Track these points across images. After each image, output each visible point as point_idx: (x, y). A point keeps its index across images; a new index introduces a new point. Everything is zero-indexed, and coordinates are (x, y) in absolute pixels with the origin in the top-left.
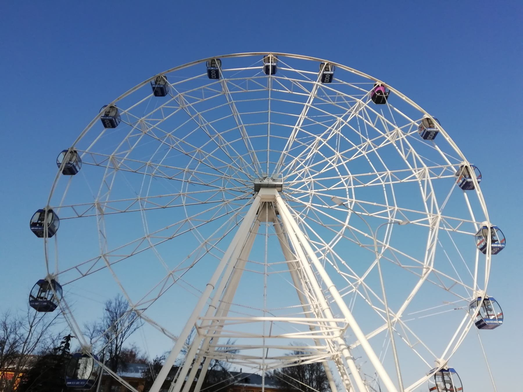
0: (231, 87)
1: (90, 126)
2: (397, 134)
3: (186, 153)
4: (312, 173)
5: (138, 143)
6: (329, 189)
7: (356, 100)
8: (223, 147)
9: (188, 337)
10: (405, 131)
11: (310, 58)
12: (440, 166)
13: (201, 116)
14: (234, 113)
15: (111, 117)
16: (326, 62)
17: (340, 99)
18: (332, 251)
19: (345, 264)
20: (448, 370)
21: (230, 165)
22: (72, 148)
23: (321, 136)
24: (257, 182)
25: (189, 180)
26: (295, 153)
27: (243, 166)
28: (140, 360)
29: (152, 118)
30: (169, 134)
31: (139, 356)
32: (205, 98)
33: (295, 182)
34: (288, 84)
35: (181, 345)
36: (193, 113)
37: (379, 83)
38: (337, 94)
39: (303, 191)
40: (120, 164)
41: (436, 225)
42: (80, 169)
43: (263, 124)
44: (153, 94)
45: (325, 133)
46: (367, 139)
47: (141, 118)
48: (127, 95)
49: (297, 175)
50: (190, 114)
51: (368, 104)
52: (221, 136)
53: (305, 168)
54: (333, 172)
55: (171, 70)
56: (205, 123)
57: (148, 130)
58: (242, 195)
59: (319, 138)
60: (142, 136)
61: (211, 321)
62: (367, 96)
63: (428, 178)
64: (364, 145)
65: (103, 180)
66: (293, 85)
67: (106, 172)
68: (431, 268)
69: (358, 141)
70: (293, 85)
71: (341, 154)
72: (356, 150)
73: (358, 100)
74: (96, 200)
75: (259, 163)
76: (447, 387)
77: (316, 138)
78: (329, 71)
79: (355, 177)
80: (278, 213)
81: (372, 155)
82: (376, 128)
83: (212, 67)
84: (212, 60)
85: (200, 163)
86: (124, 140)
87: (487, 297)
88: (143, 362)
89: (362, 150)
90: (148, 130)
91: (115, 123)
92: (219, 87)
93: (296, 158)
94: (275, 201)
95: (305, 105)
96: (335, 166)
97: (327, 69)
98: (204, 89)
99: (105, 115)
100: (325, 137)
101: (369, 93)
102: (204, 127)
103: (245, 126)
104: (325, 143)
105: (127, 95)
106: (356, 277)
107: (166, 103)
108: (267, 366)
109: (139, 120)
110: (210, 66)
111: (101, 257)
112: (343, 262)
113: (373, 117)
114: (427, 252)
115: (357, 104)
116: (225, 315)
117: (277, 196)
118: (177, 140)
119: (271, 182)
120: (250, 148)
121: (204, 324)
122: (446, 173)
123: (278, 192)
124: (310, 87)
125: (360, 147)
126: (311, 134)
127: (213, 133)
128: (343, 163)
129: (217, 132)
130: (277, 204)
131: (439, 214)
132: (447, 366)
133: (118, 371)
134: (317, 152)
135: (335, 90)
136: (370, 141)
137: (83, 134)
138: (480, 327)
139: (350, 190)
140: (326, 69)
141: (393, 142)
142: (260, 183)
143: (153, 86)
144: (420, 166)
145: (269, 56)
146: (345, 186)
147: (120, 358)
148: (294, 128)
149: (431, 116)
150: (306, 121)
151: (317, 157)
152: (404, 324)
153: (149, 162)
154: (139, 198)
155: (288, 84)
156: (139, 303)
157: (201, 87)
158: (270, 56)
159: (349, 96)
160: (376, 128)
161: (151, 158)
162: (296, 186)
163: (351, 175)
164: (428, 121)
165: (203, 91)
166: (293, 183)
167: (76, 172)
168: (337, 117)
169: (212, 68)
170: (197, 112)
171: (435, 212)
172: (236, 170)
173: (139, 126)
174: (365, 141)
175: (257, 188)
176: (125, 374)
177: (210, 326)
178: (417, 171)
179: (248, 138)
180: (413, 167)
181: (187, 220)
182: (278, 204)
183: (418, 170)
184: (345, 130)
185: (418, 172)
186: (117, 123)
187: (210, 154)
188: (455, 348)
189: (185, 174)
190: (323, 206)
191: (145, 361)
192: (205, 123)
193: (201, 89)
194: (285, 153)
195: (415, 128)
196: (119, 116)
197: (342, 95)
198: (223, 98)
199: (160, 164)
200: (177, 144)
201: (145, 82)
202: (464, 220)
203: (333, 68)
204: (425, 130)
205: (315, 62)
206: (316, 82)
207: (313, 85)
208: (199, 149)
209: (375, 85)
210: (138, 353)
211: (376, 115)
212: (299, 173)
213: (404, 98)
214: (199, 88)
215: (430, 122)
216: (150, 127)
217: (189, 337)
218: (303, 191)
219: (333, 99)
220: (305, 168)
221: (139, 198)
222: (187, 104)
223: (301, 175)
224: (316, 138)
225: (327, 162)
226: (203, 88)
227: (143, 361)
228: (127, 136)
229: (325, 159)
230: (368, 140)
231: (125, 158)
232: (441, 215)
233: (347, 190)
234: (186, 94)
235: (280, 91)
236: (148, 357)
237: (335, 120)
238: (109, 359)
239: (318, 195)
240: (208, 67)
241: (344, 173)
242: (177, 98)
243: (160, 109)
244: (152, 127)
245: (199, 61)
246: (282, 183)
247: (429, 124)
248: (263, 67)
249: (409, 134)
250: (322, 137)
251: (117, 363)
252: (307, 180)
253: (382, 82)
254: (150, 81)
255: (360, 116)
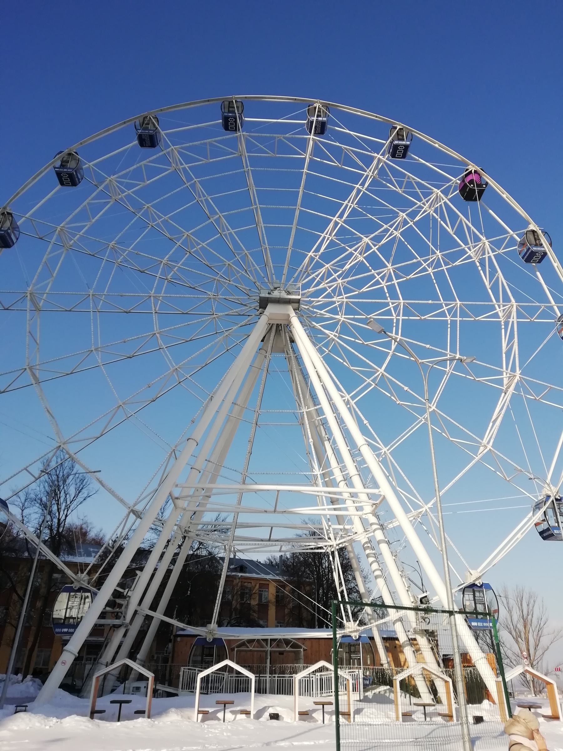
0: (250, 147)
1: (35, 178)
2: (482, 250)
3: (170, 237)
4: (347, 291)
5: (103, 214)
6: (477, 319)
7: (432, 190)
8: (225, 235)
9: (161, 509)
10: (496, 245)
11: (376, 117)
12: (538, 304)
13: (199, 186)
14: (200, 197)
15: (70, 168)
16: (399, 125)
17: (409, 185)
18: (355, 406)
19: (368, 425)
20: (481, 586)
21: (229, 263)
22: (5, 208)
23: (370, 237)
24: (264, 294)
25: (169, 277)
26: (327, 257)
27: (249, 267)
28: (93, 540)
29: (129, 180)
30: (148, 205)
31: (92, 534)
32: (211, 159)
33: (321, 299)
34: (337, 153)
35: (149, 520)
36: (189, 179)
37: (472, 167)
38: (407, 177)
39: (328, 315)
40: (73, 241)
41: (510, 389)
42: (17, 239)
43: (288, 208)
44: (136, 142)
45: (376, 233)
46: (436, 251)
47: (110, 177)
48: (94, 139)
49: (325, 290)
50: (184, 179)
51: (449, 200)
52: (223, 219)
53: (337, 281)
54: (379, 293)
55: (168, 108)
56: (204, 196)
57: (120, 196)
58: (239, 309)
59: (366, 240)
60: (111, 203)
61: (193, 490)
62: (450, 186)
63: (514, 318)
64: (432, 258)
65: (44, 260)
66: (344, 152)
67: (49, 250)
68: (489, 447)
69: (424, 251)
70: (344, 152)
71: (394, 268)
72: (419, 264)
73: (435, 190)
74: (30, 289)
75: (272, 265)
76: (478, 609)
77: (361, 238)
78: (403, 140)
79: (407, 303)
80: (292, 341)
81: (440, 275)
82: (454, 236)
83: (229, 112)
84: (229, 102)
85: (188, 254)
86: (82, 206)
87: (559, 496)
88: (97, 543)
89: (428, 265)
90: (120, 196)
91: (77, 179)
92: (234, 144)
93: (327, 266)
94: (289, 325)
95: (355, 187)
96: (384, 284)
97: (400, 137)
98: (211, 144)
99: (61, 165)
100: (377, 239)
101: (456, 181)
102: (201, 201)
103: (260, 208)
104: (375, 249)
105: (94, 139)
106: (381, 446)
107: (151, 159)
108: (234, 548)
109: (107, 178)
110: (226, 110)
111: (26, 369)
112: (365, 422)
113: (453, 218)
114: (491, 424)
115: (433, 196)
116: (213, 481)
117: (291, 316)
118: (160, 217)
119: (284, 295)
120: (264, 243)
121: (184, 494)
122: (544, 315)
123: (294, 310)
124: (368, 161)
125: (425, 261)
126: (357, 233)
127: (214, 213)
128: (395, 282)
129: (218, 211)
130: (292, 327)
131: (518, 372)
132: (480, 580)
133: (61, 554)
134: (362, 261)
135: (404, 171)
136: (441, 254)
137: (23, 189)
138: (544, 538)
139: (398, 320)
140: (399, 136)
141: (476, 259)
142: (267, 296)
143: (56, 169)
144: (506, 299)
145: (315, 105)
146: (393, 316)
147: (64, 536)
148: (332, 220)
149: (538, 228)
150: (354, 212)
151: (360, 268)
152: (433, 518)
153: (113, 243)
154: (91, 294)
155: (337, 153)
156: (70, 439)
157: (205, 141)
158: (317, 105)
159: (423, 182)
160: (454, 236)
161: (117, 238)
162: (321, 307)
163: (402, 301)
164: (534, 235)
165: (208, 147)
166: (319, 301)
167: (11, 243)
168: (399, 212)
169: (231, 114)
170: (194, 177)
171: (513, 370)
172: (238, 272)
173: (106, 187)
174: (434, 253)
175: (264, 303)
176: (70, 559)
177: (191, 496)
178: (501, 306)
179: (263, 226)
180: (498, 300)
181: (155, 334)
182: (293, 327)
183: (504, 306)
184: (408, 234)
185: (502, 308)
186: (79, 179)
187: (204, 244)
188: (496, 559)
189: (161, 267)
190: (357, 341)
191: (100, 542)
192: (204, 196)
193: (205, 144)
194: (313, 255)
195: (512, 241)
196: (82, 169)
197: (414, 179)
198: (237, 162)
199: (130, 249)
200: (158, 223)
201: (125, 123)
202: (552, 386)
203: (410, 135)
204: (529, 249)
205: (386, 123)
206: (378, 154)
207: (373, 158)
208: (187, 233)
209: (467, 170)
210: (90, 530)
211: (459, 216)
212: (330, 287)
213: (504, 196)
214: (202, 142)
215: (536, 237)
216: (123, 192)
217: (163, 510)
218: (328, 315)
219: (400, 184)
220: (338, 282)
221: (91, 294)
222: (182, 164)
223: (331, 291)
224: (361, 238)
225: (373, 277)
226: (209, 142)
227: (97, 542)
228: (87, 201)
229: (371, 271)
230: (438, 252)
231: (81, 233)
232: (520, 374)
233: (395, 321)
234: (182, 148)
235: (324, 161)
236: (104, 536)
237: (396, 215)
238: (49, 538)
239: (349, 323)
240: (223, 113)
241: (394, 296)
242: (168, 153)
243: (141, 166)
244: (126, 193)
245: (208, 101)
246: (299, 297)
247: (535, 240)
248: (305, 122)
249: (501, 251)
250: (371, 239)
251: (60, 543)
252: (339, 300)
253: (477, 167)
254: (53, 165)
255: (435, 214)
